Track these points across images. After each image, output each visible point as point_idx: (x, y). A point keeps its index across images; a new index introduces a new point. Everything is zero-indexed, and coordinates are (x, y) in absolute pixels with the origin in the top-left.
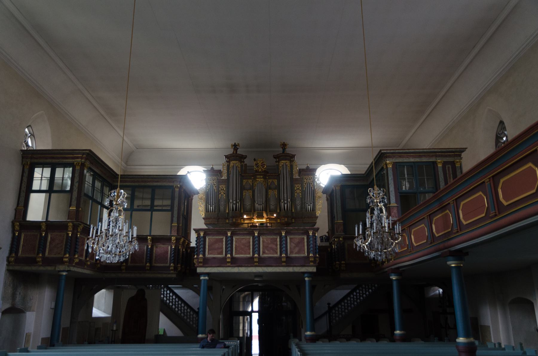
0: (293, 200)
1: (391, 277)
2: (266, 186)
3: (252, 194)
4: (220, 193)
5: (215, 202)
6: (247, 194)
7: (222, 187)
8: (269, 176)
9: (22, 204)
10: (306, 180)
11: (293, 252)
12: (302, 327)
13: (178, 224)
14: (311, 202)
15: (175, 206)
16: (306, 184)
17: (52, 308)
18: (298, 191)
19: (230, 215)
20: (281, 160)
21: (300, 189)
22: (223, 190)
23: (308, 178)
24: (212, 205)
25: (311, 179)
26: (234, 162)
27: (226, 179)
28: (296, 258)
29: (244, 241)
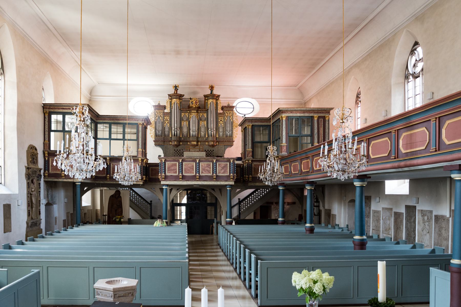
0: (217, 129)
1: (279, 188)
4: (165, 123)
6: (185, 124)
7: (167, 118)
8: (200, 110)
9: (47, 139)
11: (220, 172)
12: (222, 215)
14: (230, 131)
15: (140, 137)
16: (227, 117)
17: (65, 202)
18: (221, 122)
19: (173, 139)
21: (223, 120)
22: (167, 120)
23: (229, 113)
24: (159, 132)
27: (169, 112)
28: (222, 176)
29: (189, 165)
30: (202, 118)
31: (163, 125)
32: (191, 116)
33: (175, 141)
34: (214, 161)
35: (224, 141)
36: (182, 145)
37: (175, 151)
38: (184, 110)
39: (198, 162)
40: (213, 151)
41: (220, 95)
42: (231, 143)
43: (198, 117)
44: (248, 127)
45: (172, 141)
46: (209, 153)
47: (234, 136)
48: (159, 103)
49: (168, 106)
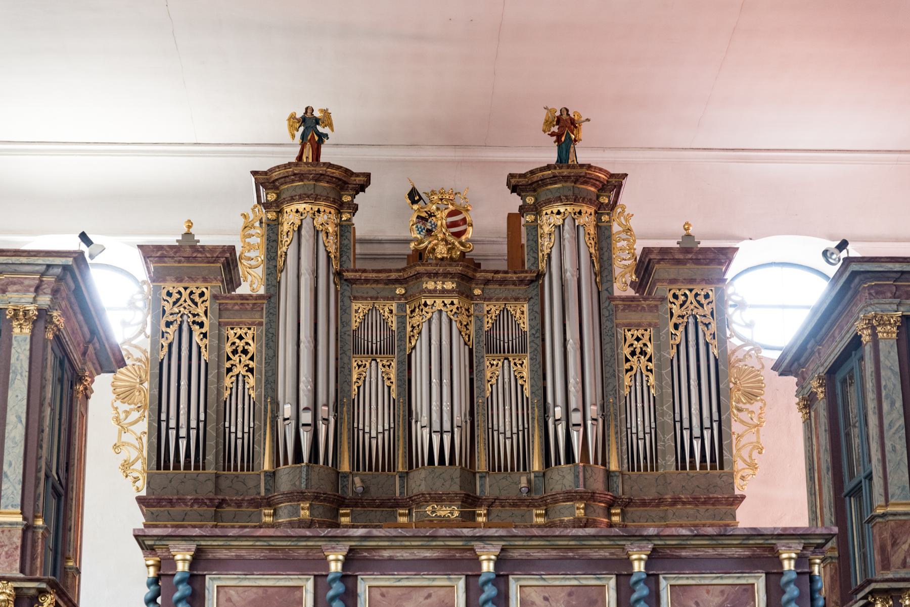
2: (473, 335)
3: (399, 379)
4: (229, 370)
5: (202, 417)
7: (240, 338)
8: (487, 282)
10: (681, 306)
13: (25, 519)
16: (681, 328)
20: (549, 202)
21: (650, 350)
22: (245, 352)
23: (691, 296)
25: (703, 301)
26: (301, 207)
27: (261, 297)
30: (496, 333)
31: (212, 387)
32: (416, 320)
33: (297, 496)
34: (629, 563)
35: (668, 497)
38: (367, 281)
39: (488, 567)
41: (626, 175)
42: (723, 509)
43: (472, 328)
44: (874, 335)
47: (739, 465)
48: (188, 235)
49: (252, 254)
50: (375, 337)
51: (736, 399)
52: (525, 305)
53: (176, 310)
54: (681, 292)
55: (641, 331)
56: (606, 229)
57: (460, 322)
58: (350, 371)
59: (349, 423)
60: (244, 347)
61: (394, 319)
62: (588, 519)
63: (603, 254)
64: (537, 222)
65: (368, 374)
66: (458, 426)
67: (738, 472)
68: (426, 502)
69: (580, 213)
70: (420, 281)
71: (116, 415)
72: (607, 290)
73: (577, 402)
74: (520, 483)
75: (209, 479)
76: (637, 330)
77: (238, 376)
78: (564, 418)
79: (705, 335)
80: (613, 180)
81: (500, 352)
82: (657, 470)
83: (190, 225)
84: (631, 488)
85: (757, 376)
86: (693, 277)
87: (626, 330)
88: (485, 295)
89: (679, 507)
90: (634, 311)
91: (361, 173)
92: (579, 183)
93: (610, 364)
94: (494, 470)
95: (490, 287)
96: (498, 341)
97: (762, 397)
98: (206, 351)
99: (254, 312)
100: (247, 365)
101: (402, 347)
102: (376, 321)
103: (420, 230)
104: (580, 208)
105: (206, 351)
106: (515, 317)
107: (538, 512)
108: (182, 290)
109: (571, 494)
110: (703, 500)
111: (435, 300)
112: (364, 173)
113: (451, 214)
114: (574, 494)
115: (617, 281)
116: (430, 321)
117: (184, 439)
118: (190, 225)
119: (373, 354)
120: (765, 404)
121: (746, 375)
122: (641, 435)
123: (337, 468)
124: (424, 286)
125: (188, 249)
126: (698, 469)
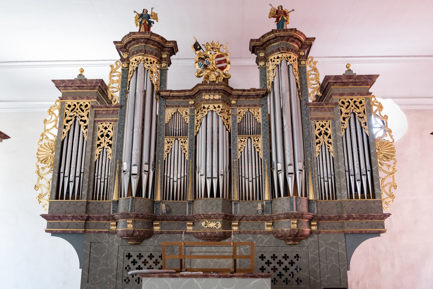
7: (106, 128)
10: (347, 108)
16: (347, 120)
18: (324, 139)
20: (272, 53)
21: (330, 132)
22: (108, 136)
23: (352, 103)
25: (359, 105)
26: (137, 58)
32: (199, 117)
33: (126, 216)
35: (345, 215)
36: (161, 233)
37: (131, 259)
38: (173, 97)
40: (265, 260)
41: (315, 38)
43: (230, 121)
45: (116, 216)
46: (280, 269)
47: (384, 196)
49: (115, 85)
50: (177, 127)
51: (379, 159)
52: (260, 109)
53: (72, 114)
54: (347, 100)
55: (324, 122)
56: (304, 68)
57: (223, 117)
58: (163, 145)
59: (161, 173)
60: (107, 133)
61: (188, 117)
62: (299, 230)
63: (302, 81)
64: (266, 65)
65: (173, 146)
66: (221, 175)
67: (383, 200)
68: (201, 219)
69: (290, 57)
70: (201, 95)
71: (38, 170)
72: (305, 100)
73: (291, 161)
74: (257, 207)
75: (83, 205)
76: (322, 121)
77: (103, 148)
78: (283, 170)
79: (360, 123)
80: (307, 42)
81: (246, 134)
82: (336, 199)
83: (82, 71)
84: (322, 209)
85: (391, 145)
86: (353, 92)
87: (316, 121)
88: (238, 104)
89: (351, 220)
90: (320, 111)
91: (171, 41)
92: (289, 41)
93: (308, 140)
94: (242, 199)
95: (241, 99)
96: (245, 128)
97: (394, 157)
98: (86, 135)
99: (114, 115)
100: (108, 143)
101: (192, 132)
102: (256, 168)
103: (200, 65)
104: (290, 55)
105: (86, 135)
106: (254, 115)
107: (268, 224)
108: (76, 104)
109: (289, 215)
110: (366, 217)
111: (209, 105)
112: (173, 41)
113: (218, 57)
114: (291, 215)
115: (310, 96)
116: (206, 116)
117: (72, 183)
118: (82, 71)
119: (176, 136)
120: (396, 161)
121: (384, 146)
122: (326, 179)
123: (153, 199)
124: (203, 97)
125: (78, 82)
126: (360, 198)
